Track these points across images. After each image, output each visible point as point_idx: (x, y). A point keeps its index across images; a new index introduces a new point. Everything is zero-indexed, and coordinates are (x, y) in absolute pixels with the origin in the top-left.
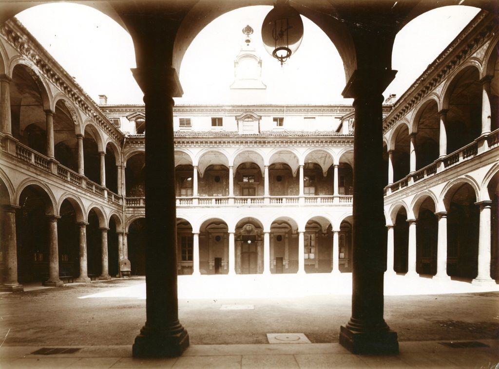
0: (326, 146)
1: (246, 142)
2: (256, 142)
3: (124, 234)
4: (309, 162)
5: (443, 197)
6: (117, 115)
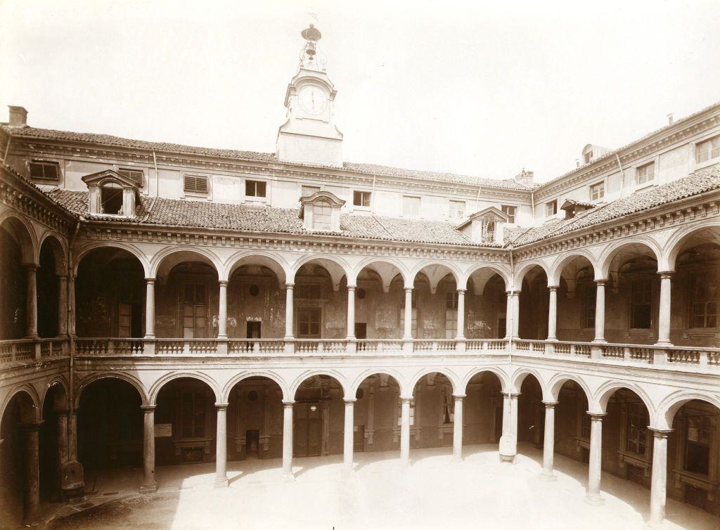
0: (448, 258)
2: (335, 246)
3: (72, 412)
5: (666, 408)
6: (54, 156)
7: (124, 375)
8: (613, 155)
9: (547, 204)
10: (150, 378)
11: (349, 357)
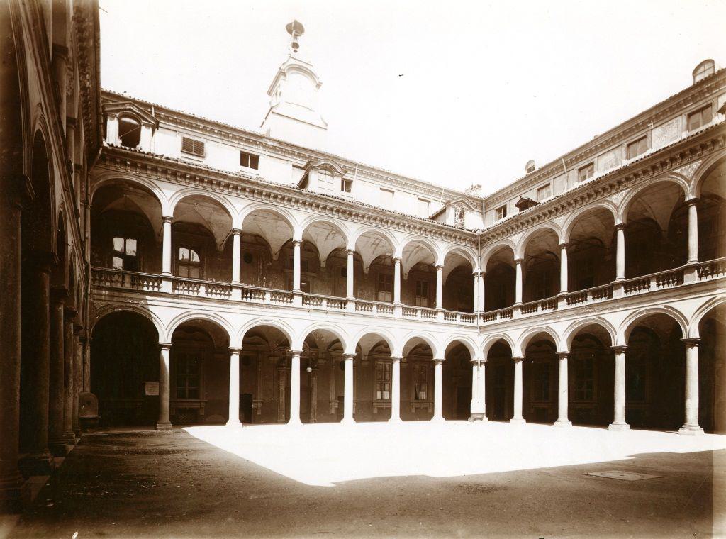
1: (324, 208)
2: (338, 211)
4: (387, 254)
5: (625, 328)
7: (142, 308)
8: (560, 159)
9: (497, 210)
10: (167, 314)
11: (350, 314)
